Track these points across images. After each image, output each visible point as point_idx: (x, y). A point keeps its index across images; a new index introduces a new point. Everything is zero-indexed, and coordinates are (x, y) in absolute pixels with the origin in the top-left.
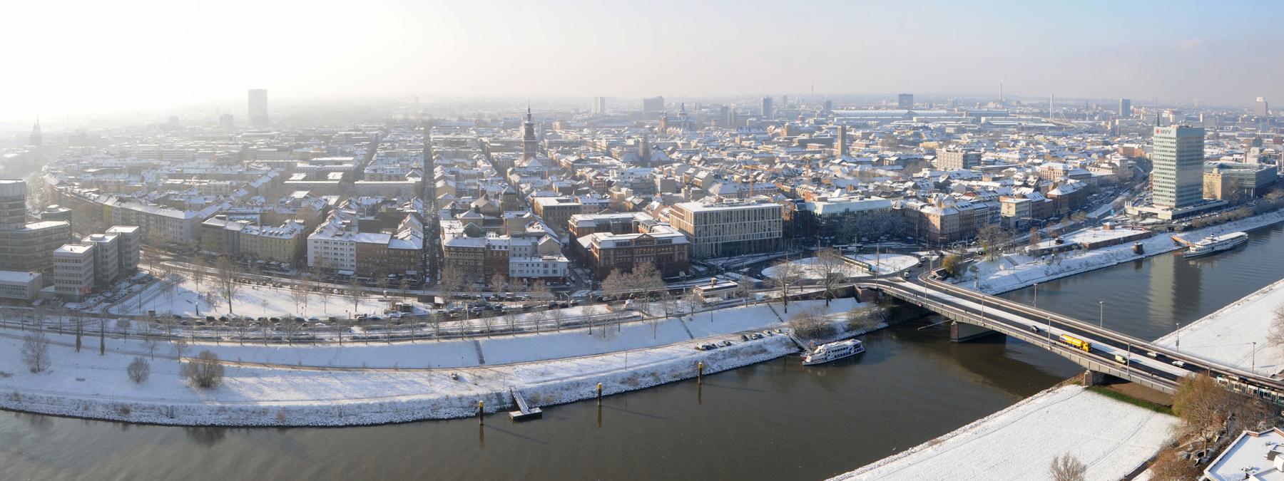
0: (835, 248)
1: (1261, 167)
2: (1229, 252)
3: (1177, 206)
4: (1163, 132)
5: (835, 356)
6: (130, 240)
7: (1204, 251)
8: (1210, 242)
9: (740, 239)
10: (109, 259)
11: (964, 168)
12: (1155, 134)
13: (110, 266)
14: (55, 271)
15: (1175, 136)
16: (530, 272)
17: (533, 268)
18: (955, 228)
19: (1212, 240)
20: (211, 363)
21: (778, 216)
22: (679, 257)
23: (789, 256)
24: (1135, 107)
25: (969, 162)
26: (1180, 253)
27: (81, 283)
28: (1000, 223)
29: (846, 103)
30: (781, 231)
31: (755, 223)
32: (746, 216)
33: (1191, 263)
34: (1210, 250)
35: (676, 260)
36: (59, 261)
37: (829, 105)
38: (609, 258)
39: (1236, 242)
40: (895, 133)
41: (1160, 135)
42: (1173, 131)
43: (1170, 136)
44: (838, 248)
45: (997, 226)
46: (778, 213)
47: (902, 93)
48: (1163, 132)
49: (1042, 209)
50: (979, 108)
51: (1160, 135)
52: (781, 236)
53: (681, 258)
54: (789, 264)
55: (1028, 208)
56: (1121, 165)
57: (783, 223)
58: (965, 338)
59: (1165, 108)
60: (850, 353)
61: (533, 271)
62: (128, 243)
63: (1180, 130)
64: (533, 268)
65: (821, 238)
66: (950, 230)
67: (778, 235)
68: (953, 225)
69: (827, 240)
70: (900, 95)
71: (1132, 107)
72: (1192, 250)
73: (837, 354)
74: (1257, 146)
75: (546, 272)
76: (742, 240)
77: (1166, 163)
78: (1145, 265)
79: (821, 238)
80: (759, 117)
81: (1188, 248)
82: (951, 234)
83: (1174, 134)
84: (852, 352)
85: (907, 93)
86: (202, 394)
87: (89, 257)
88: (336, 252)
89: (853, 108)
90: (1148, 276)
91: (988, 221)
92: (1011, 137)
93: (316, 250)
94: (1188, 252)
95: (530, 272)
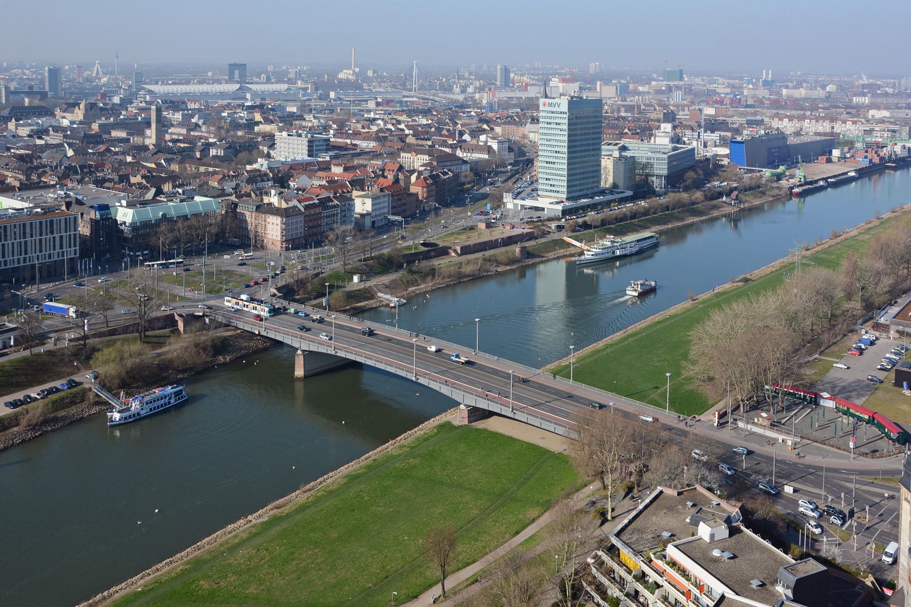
0: (149, 266)
1: (675, 149)
2: (634, 258)
3: (568, 199)
4: (550, 105)
5: (151, 410)
7: (602, 256)
8: (609, 244)
9: (19, 263)
11: (309, 156)
12: (541, 108)
15: (566, 110)
18: (299, 231)
19: (612, 242)
21: (72, 228)
24: (516, 74)
25: (315, 148)
26: (573, 259)
28: (353, 224)
29: (162, 77)
30: (78, 248)
31: (14, 259)
32: (28, 230)
33: (588, 271)
34: (610, 255)
37: (140, 78)
39: (645, 244)
40: (223, 114)
41: (547, 108)
42: (564, 105)
43: (560, 110)
44: (153, 265)
45: (350, 227)
46: (72, 224)
47: (232, 62)
48: (550, 105)
49: (405, 204)
50: (55, 345)
51: (547, 108)
52: (78, 255)
55: (386, 204)
56: (499, 147)
57: (80, 238)
59: (554, 75)
60: (169, 403)
63: (571, 104)
65: (132, 254)
66: (292, 235)
67: (73, 253)
68: (296, 228)
69: (139, 256)
70: (230, 65)
71: (512, 75)
72: (588, 256)
73: (152, 406)
74: (669, 122)
76: (22, 264)
78: (529, 273)
79: (132, 254)
80: (43, 95)
81: (582, 253)
83: (564, 107)
84: (172, 401)
85: (238, 62)
89: (170, 82)
90: (533, 288)
91: (339, 221)
92: (366, 116)
94: (583, 257)
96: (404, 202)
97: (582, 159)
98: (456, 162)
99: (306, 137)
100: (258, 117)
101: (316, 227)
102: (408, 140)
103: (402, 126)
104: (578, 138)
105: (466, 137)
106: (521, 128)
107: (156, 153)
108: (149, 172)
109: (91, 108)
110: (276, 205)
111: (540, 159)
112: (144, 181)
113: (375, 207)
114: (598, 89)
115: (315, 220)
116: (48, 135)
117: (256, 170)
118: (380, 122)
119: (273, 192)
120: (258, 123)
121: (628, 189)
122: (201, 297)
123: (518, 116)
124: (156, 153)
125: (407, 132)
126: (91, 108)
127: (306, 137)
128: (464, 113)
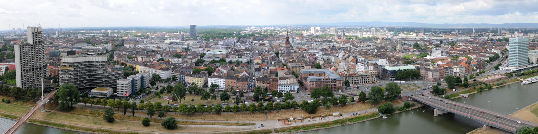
4: (513, 40)
6: (145, 77)
10: (137, 84)
13: (137, 86)
14: (117, 88)
16: (285, 89)
17: (286, 88)
20: (12, 88)
22: (339, 85)
23: (357, 82)
27: (127, 92)
35: (338, 86)
36: (119, 84)
38: (314, 85)
53: (340, 85)
54: (17, 38)
58: (503, 121)
61: (286, 89)
62: (144, 78)
64: (286, 88)
68: (437, 76)
72: (524, 83)
75: (291, 89)
77: (513, 44)
82: (436, 79)
86: (263, 128)
87: (130, 83)
88: (218, 82)
93: (211, 82)
95: (285, 89)
96: (469, 69)
97: (523, 46)
98: (485, 57)
99: (441, 50)
100: (428, 44)
101: (442, 75)
102: (471, 51)
103: (469, 47)
104: (521, 46)
105: (488, 50)
106: (505, 47)
107: (399, 52)
108: (397, 57)
109: (382, 39)
110: (431, 69)
111: (510, 56)
112: (395, 60)
113: (460, 70)
114: (529, 35)
115: (442, 73)
116: (371, 46)
117: (426, 59)
118: (463, 46)
119: (430, 65)
120: (428, 46)
121: (537, 64)
122: (409, 92)
123: (504, 43)
124: (399, 52)
125: (470, 49)
126: (382, 39)
127: (441, 50)
128: (487, 43)
